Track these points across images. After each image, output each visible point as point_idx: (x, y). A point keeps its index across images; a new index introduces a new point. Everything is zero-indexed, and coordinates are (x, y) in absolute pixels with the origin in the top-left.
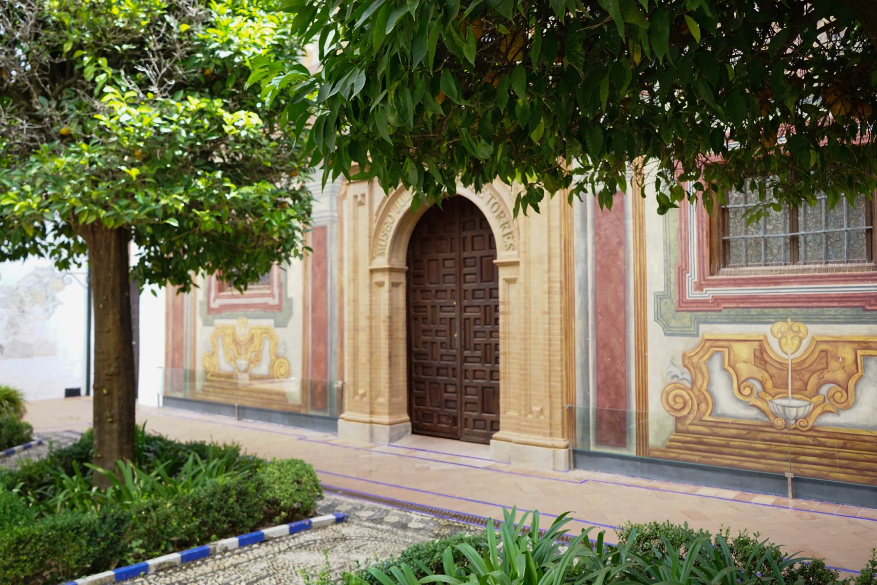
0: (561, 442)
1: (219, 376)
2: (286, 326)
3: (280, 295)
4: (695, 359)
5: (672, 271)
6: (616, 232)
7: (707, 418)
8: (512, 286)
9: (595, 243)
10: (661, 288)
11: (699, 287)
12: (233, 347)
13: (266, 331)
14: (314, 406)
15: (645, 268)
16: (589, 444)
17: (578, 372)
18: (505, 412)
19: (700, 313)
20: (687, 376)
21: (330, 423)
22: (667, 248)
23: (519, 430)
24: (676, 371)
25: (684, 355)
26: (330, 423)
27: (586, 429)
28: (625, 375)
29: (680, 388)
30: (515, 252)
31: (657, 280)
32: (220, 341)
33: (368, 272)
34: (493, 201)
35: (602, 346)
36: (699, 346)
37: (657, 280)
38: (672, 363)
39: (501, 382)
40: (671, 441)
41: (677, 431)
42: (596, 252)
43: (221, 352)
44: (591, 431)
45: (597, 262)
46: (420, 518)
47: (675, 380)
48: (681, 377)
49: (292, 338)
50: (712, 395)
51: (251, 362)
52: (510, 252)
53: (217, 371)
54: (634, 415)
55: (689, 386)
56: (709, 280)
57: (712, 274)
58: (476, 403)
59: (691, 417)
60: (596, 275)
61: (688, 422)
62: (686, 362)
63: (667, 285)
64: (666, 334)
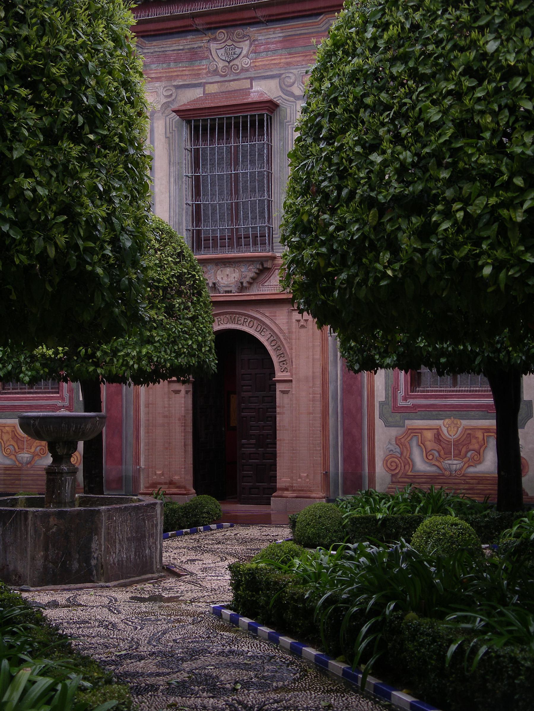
4: (403, 440)
7: (409, 473)
11: (405, 399)
18: (281, 479)
20: (398, 450)
24: (392, 447)
25: (396, 438)
28: (361, 451)
30: (288, 374)
34: (272, 338)
35: (347, 433)
38: (390, 443)
40: (389, 488)
41: (393, 482)
47: (391, 452)
52: (284, 374)
60: (343, 390)
61: (399, 476)
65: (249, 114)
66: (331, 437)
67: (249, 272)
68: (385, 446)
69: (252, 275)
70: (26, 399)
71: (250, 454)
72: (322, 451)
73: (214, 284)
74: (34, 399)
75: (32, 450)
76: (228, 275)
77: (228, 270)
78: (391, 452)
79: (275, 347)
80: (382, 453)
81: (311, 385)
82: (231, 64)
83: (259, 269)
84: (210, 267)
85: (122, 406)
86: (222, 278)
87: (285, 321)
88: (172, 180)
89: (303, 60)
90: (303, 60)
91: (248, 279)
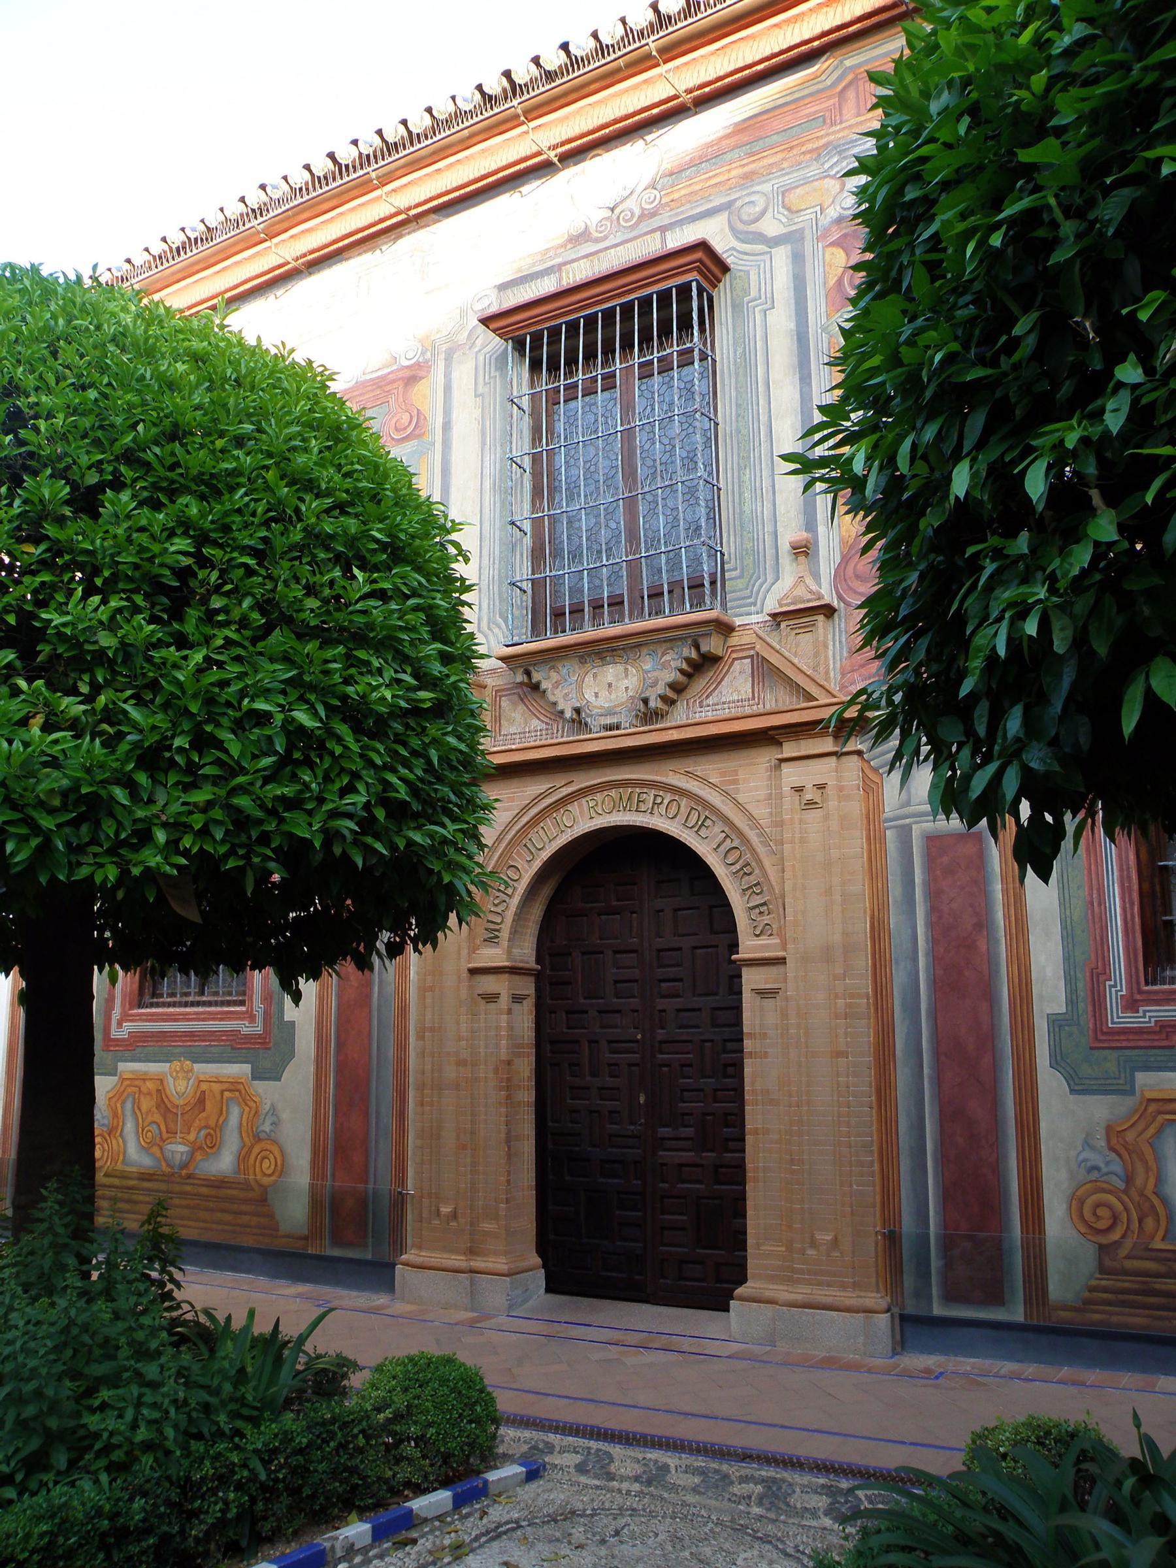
0: (875, 1299)
1: (123, 1176)
2: (279, 1080)
3: (267, 1015)
4: (1130, 1136)
5: (1079, 975)
6: (971, 905)
7: (1158, 1244)
8: (769, 1003)
9: (931, 925)
10: (1059, 1006)
11: (1131, 1004)
12: (157, 1117)
13: (234, 1086)
14: (338, 1239)
15: (1028, 971)
16: (929, 1298)
17: (905, 1164)
18: (758, 1245)
19: (1136, 1052)
20: (1117, 1167)
21: (379, 1273)
22: (1068, 935)
23: (791, 1281)
24: (1096, 1159)
25: (1109, 1129)
26: (379, 1273)
27: (923, 1273)
28: (998, 1169)
29: (1104, 1191)
30: (775, 941)
31: (1050, 991)
32: (129, 1105)
33: (465, 974)
34: (728, 844)
35: (952, 1114)
36: (1136, 1111)
37: (1050, 991)
38: (1087, 1144)
39: (749, 1187)
40: (1092, 1289)
41: (1103, 1270)
42: (934, 942)
43: (129, 1126)
44: (934, 1280)
45: (936, 959)
46: (684, 1463)
47: (1095, 1175)
48: (1105, 1170)
49: (292, 1100)
50: (1165, 1202)
51: (196, 1148)
52: (763, 941)
53: (119, 1167)
54: (1019, 1243)
55: (1121, 1185)
56: (1149, 992)
57: (1147, 984)
58: (684, 1229)
59: (1128, 1243)
60: (936, 984)
61: (1123, 1252)
62: (1114, 1141)
63: (1071, 1002)
64: (1072, 1091)
65: (655, 288)
66: (903, 1125)
67: (663, 668)
68: (1073, 1153)
69: (671, 676)
70: (186, 1018)
71: (681, 1165)
72: (876, 1167)
73: (578, 711)
74: (198, 1017)
75: (192, 1137)
76: (610, 685)
77: (611, 672)
78: (1095, 1175)
79: (738, 866)
80: (1063, 1175)
81: (839, 970)
82: (617, 211)
83: (688, 660)
84: (569, 670)
85: (370, 1034)
86: (596, 695)
87: (762, 793)
88: (487, 485)
89: (784, 159)
90: (784, 159)
91: (661, 689)
